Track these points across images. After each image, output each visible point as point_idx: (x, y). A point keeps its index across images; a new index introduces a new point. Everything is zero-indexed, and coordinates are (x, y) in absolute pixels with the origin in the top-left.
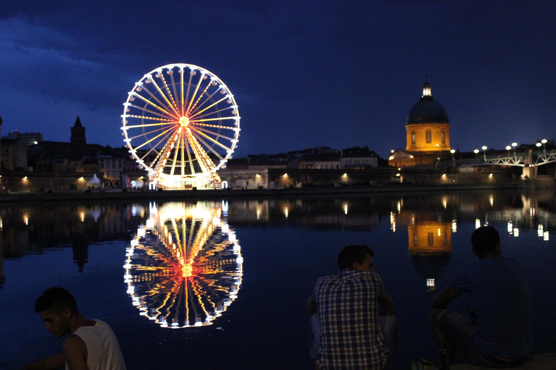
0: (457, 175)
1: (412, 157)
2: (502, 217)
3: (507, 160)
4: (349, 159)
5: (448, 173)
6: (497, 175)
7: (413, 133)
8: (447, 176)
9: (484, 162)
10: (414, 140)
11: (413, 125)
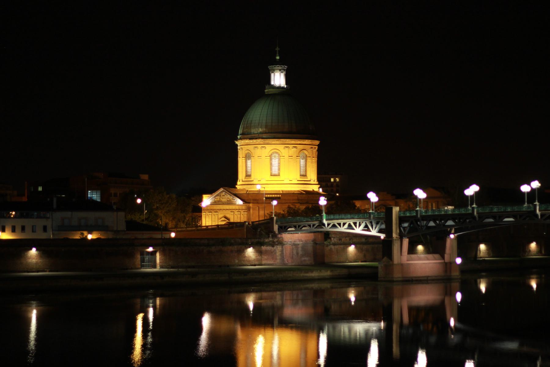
0: (278, 248)
1: (239, 202)
2: (350, 331)
3: (344, 224)
4: (68, 214)
5: (257, 245)
6: (365, 247)
7: (248, 157)
8: (259, 252)
9: (324, 225)
10: (249, 169)
11: (247, 141)
